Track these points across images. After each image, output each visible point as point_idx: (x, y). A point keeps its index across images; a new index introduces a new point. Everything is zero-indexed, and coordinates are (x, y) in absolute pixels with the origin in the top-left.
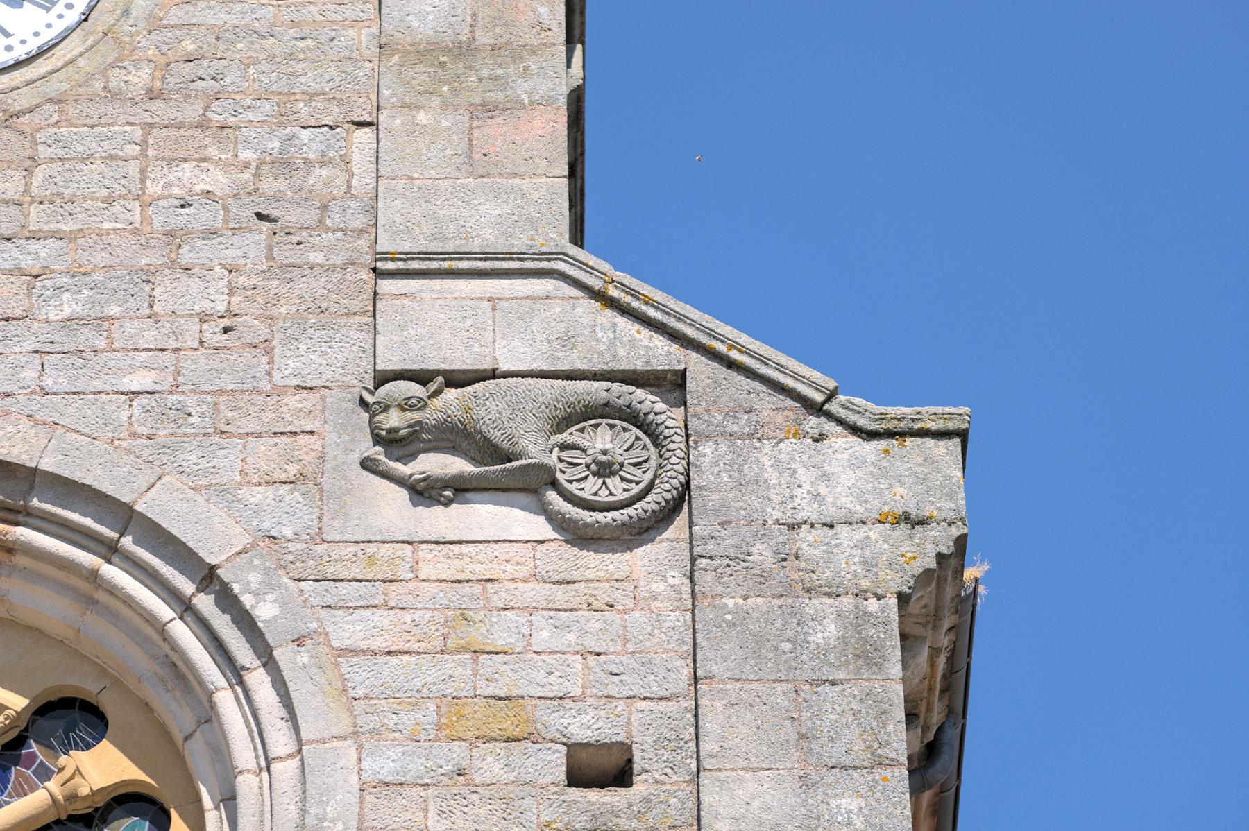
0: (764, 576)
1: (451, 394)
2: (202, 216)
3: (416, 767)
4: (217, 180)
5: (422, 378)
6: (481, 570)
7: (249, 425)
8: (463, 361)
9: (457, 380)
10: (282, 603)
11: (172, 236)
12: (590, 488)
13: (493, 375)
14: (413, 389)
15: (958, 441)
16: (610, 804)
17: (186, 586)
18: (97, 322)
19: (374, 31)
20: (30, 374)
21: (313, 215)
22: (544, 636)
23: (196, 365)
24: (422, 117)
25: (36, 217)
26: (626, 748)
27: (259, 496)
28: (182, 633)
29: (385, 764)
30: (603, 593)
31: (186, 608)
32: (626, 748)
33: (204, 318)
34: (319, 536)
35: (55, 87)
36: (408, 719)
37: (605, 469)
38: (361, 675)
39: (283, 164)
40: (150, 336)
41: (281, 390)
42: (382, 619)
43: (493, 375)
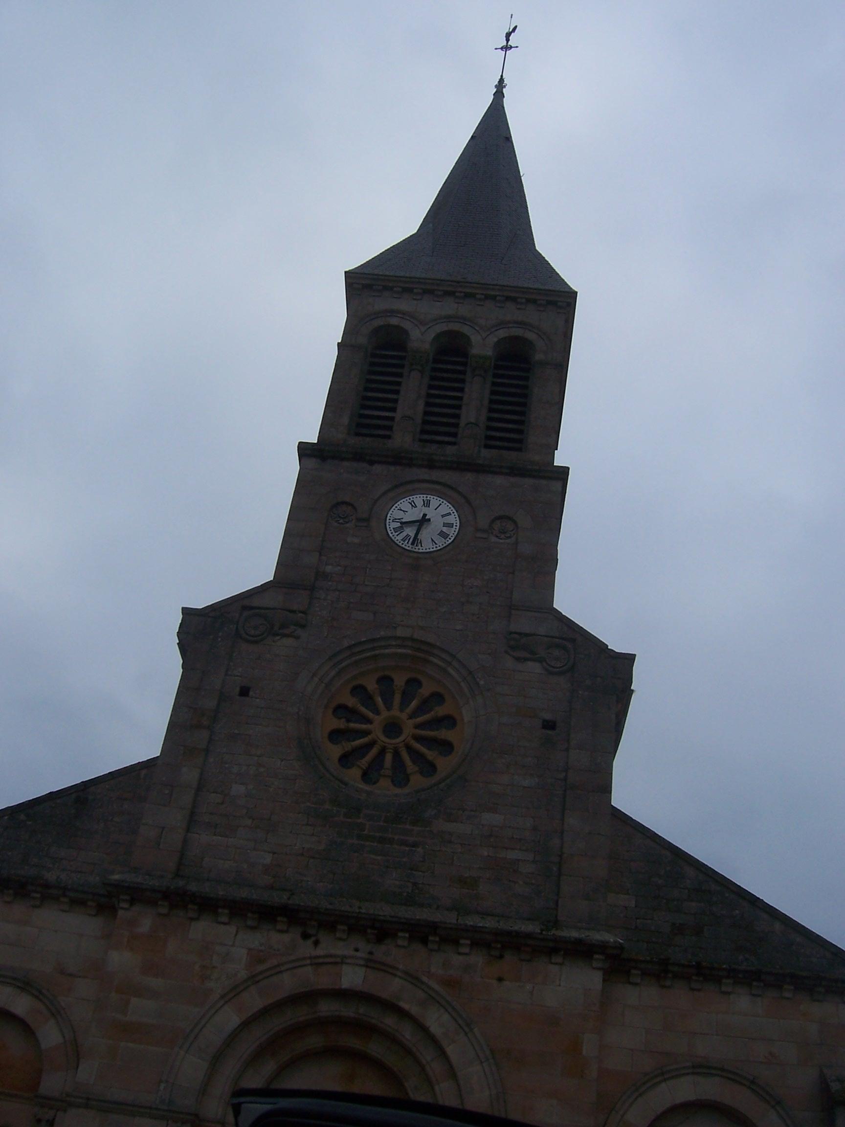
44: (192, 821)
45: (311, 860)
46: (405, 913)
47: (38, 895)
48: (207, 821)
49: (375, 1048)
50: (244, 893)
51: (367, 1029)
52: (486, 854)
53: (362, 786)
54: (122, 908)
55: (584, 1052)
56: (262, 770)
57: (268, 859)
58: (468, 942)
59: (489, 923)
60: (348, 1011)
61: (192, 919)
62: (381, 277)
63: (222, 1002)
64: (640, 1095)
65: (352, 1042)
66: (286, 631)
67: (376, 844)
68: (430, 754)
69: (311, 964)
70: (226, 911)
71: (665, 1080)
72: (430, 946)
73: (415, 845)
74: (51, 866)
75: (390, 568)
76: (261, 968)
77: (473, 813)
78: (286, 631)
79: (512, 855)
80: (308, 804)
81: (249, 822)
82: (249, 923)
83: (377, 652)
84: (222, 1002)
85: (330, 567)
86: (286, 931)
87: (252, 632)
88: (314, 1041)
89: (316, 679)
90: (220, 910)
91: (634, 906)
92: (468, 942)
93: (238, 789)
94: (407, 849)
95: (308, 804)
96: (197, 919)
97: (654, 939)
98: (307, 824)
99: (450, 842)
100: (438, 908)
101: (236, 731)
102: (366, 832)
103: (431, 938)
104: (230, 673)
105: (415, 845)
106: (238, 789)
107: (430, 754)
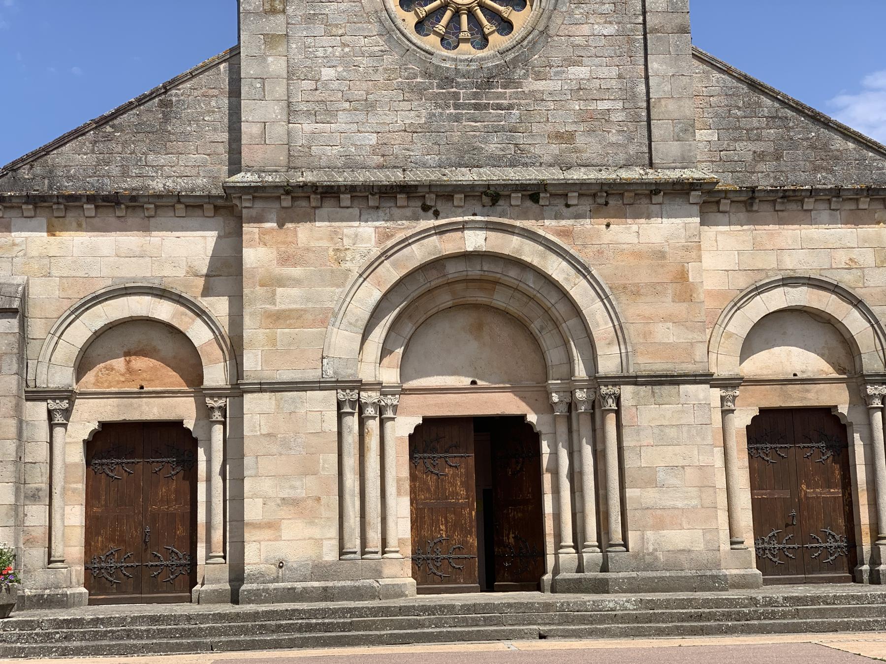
44: (291, 111)
45: (415, 135)
46: (514, 175)
47: (153, 206)
48: (305, 109)
49: (500, 299)
50: (361, 177)
51: (493, 284)
52: (577, 108)
53: (445, 53)
54: (245, 207)
55: (691, 280)
56: (347, 50)
57: (373, 139)
58: (576, 194)
59: (592, 175)
60: (474, 271)
61: (315, 208)
62: (238, 184)
63: (361, 280)
64: (739, 309)
65: (481, 297)
67: (472, 111)
68: (488, 27)
69: (436, 234)
70: (403, 196)
71: (759, 294)
72: (542, 202)
73: (510, 107)
74: (154, 174)
76: (390, 244)
77: (559, 69)
79: (603, 106)
80: (400, 80)
81: (347, 105)
82: (371, 203)
84: (361, 280)
86: (408, 206)
88: (445, 299)
90: (342, 196)
91: (716, 139)
92: (576, 194)
93: (327, 73)
94: (503, 112)
95: (400, 80)
96: (321, 207)
97: (738, 169)
98: (404, 100)
99: (543, 100)
100: (541, 164)
101: (312, 12)
102: (461, 101)
103: (542, 195)
105: (510, 107)
106: (327, 73)
107: (488, 27)
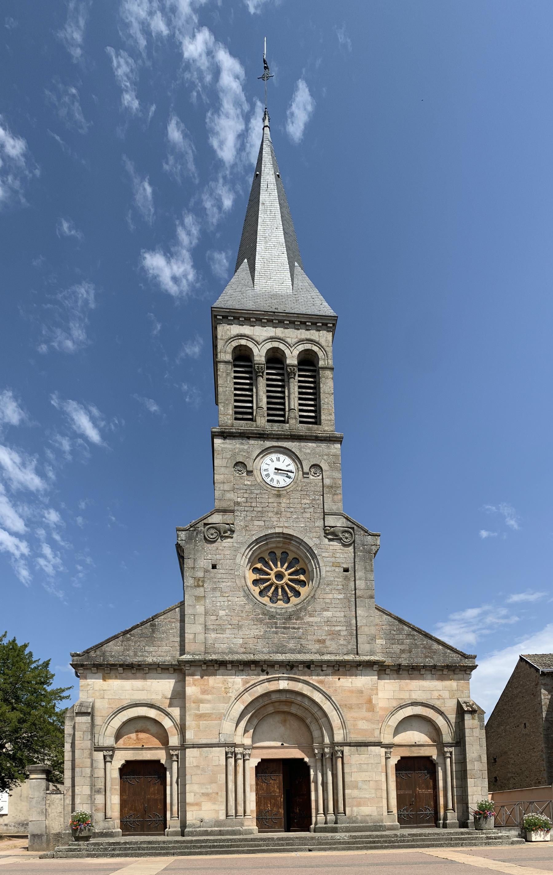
0: (362, 551)
1: (332, 529)
2: (307, 506)
3: (330, 569)
4: (308, 502)
5: (329, 527)
6: (335, 548)
7: (313, 531)
8: (333, 525)
9: (333, 527)
10: (317, 551)
11: (305, 508)
12: (345, 540)
13: (336, 527)
14: (329, 528)
15: (326, 525)
16: (437, 670)
17: (317, 567)
18: (298, 518)
19: (318, 489)
20: (292, 524)
21: (318, 506)
22: (341, 556)
23: (308, 524)
24: (328, 495)
25: (291, 505)
26: (348, 568)
27: (314, 539)
28: (315, 570)
29: (328, 569)
30: (346, 551)
31: (316, 568)
32: (348, 568)
33: (308, 518)
34: (320, 544)
35: (291, 489)
36: (329, 564)
37: (347, 538)
38: (325, 559)
39: (314, 500)
40: (303, 520)
41: (316, 527)
42: (326, 553)
43: (336, 527)
66: (226, 535)
75: (267, 497)
78: (226, 535)
83: (268, 541)
85: (239, 499)
87: (211, 537)
89: (244, 557)
104: (205, 558)
